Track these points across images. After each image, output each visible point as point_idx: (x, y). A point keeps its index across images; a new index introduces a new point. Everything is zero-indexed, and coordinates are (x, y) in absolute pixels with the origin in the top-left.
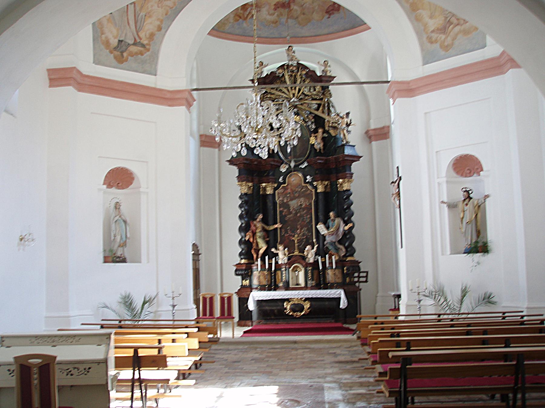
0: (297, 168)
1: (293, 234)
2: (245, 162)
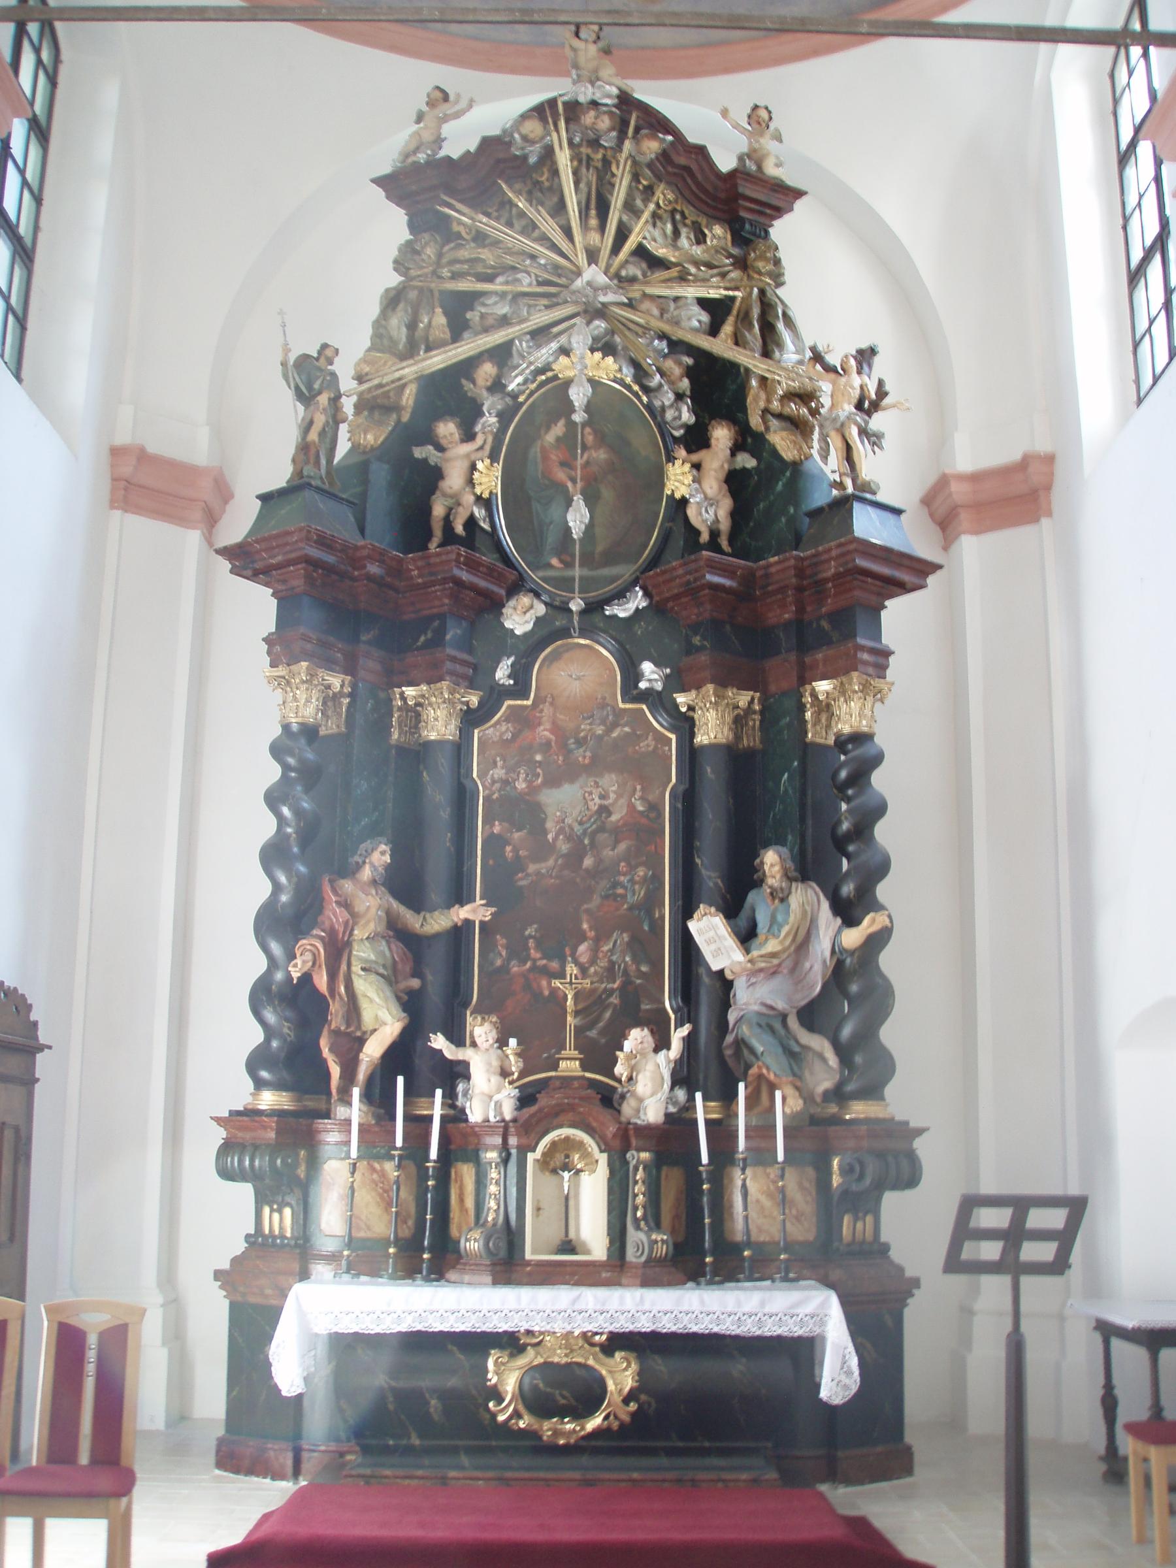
0: (596, 619)
1: (554, 965)
2: (314, 552)
